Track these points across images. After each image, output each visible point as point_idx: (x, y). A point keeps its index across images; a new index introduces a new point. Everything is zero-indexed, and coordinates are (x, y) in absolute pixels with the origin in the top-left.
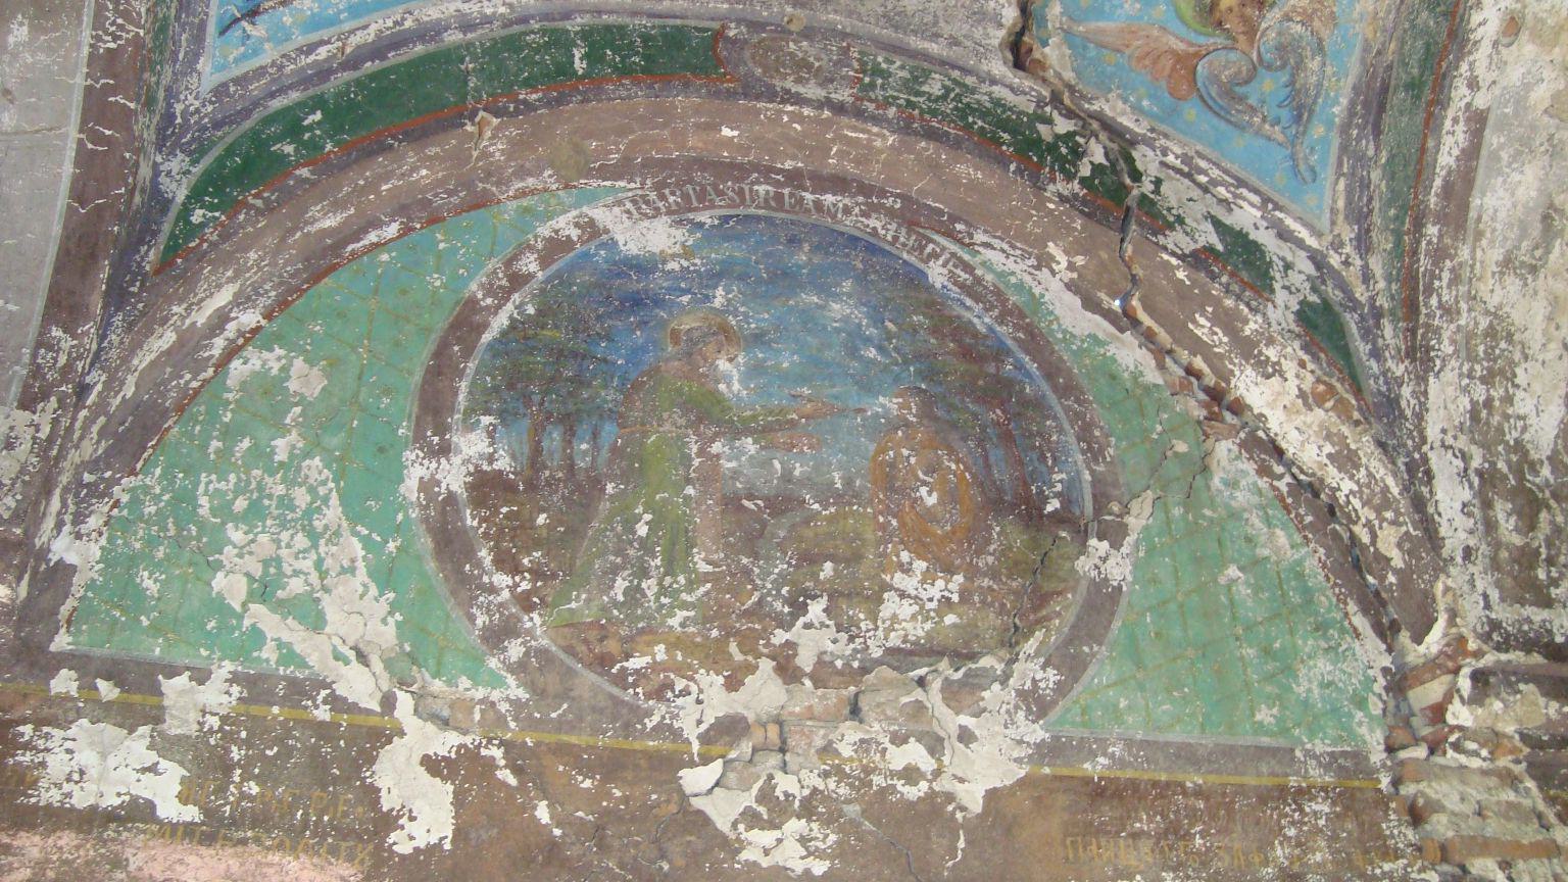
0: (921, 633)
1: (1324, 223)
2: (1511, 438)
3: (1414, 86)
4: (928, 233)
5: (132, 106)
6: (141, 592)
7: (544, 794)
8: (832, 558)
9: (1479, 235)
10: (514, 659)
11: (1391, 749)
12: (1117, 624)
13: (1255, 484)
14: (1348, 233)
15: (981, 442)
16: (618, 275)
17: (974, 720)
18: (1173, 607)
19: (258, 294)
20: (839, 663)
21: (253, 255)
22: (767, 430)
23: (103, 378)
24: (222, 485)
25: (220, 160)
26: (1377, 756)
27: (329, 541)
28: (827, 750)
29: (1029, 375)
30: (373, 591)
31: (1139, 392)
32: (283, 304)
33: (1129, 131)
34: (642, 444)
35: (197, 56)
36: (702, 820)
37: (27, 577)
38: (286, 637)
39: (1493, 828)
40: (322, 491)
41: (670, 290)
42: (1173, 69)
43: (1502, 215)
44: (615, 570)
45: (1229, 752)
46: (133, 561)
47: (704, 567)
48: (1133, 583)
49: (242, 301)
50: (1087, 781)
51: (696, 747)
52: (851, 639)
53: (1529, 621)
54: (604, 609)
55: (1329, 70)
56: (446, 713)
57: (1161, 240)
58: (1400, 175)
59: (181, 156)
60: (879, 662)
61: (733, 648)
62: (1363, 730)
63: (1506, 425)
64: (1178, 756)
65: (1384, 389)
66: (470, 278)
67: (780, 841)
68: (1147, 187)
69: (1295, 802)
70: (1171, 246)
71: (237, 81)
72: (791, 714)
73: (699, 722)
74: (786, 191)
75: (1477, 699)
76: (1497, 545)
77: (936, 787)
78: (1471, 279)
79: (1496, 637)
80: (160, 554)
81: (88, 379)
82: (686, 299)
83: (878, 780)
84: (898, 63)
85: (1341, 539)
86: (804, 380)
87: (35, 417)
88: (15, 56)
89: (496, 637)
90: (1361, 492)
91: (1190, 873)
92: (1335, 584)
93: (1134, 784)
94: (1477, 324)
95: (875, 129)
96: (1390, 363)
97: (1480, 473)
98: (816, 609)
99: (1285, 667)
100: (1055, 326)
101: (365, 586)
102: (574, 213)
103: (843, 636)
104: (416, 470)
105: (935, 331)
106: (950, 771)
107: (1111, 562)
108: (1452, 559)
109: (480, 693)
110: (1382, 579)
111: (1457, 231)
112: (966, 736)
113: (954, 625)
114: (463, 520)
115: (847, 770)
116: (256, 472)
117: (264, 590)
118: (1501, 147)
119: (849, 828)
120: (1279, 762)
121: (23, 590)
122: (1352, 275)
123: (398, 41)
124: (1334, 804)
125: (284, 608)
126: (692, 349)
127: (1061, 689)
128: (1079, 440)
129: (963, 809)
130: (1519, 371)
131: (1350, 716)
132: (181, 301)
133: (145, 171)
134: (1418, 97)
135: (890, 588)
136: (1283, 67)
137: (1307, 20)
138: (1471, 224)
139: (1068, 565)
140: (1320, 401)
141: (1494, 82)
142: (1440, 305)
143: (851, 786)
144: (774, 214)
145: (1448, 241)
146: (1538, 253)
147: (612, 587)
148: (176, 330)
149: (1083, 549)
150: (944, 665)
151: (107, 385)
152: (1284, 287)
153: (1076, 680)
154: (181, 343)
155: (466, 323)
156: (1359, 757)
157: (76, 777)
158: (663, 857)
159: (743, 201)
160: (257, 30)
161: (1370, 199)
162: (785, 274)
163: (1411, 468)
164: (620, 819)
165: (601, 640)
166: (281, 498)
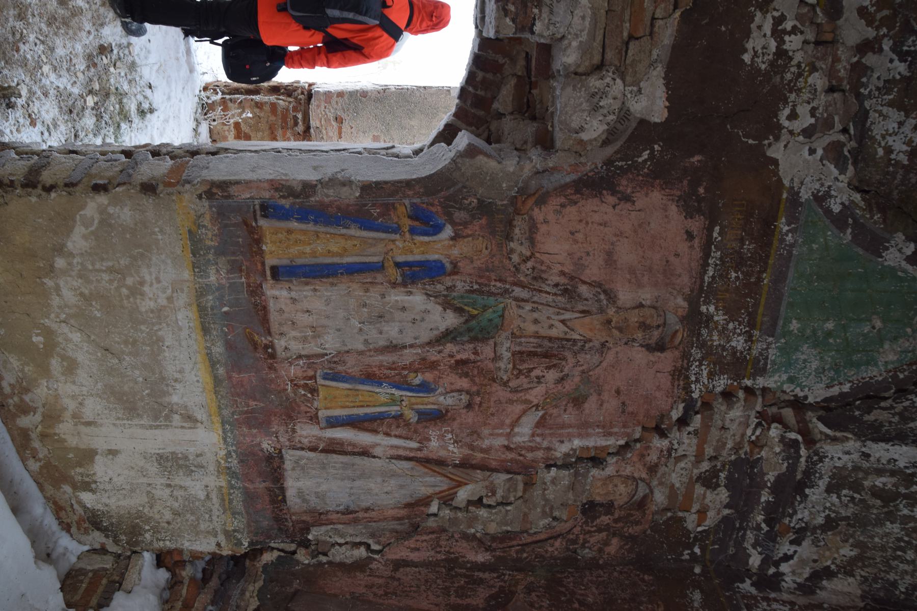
0: (875, 132)
11: (765, 390)
12: (860, 251)
17: (819, 158)
20: (864, 80)
26: (761, 382)
28: (813, 69)
39: (715, 433)
48: (882, 265)
50: (775, 219)
52: (878, 89)
53: (821, 478)
60: (861, 105)
61: (886, 12)
62: (776, 378)
67: (765, 35)
72: (838, 49)
75: (782, 439)
76: (867, 472)
79: (815, 458)
83: (793, 96)
85: (885, 392)
91: (718, 267)
92: (860, 382)
93: (769, 244)
103: (881, 84)
107: (898, 255)
108: (865, 446)
110: (858, 408)
112: (812, 152)
113: (876, 153)
115: (801, 80)
124: (742, 353)
127: (828, 212)
129: (770, 145)
131: (786, 372)
135: (907, 116)
143: (790, 81)
150: (853, 144)
153: (832, 221)
156: (762, 371)
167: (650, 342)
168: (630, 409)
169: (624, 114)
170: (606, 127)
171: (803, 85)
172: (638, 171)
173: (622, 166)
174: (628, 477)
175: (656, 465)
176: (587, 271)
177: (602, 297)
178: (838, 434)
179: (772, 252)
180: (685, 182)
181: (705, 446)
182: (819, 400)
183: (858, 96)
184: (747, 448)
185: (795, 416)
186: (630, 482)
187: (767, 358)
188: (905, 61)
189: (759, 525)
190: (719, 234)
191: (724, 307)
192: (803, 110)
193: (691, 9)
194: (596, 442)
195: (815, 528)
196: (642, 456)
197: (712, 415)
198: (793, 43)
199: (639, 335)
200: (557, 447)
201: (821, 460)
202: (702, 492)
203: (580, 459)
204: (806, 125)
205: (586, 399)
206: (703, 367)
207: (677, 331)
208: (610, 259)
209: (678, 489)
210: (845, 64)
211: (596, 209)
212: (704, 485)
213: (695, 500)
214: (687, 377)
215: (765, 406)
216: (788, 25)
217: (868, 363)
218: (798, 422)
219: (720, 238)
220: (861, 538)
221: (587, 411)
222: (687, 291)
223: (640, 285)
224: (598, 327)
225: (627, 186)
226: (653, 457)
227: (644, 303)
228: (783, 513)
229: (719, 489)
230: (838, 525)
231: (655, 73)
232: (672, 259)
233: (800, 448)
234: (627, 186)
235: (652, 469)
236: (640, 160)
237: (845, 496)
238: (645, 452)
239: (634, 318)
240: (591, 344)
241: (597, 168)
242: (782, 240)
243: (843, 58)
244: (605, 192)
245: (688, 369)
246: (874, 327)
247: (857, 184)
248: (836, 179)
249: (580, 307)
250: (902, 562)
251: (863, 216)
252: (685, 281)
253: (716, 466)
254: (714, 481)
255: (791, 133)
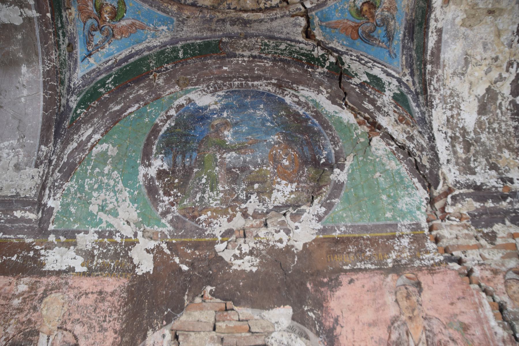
1: (400, 70)
2: (461, 126)
3: (420, 24)
4: (285, 88)
5: (55, 84)
6: (70, 212)
7: (177, 255)
8: (258, 183)
9: (444, 66)
10: (169, 219)
11: (428, 221)
13: (385, 148)
14: (407, 71)
15: (301, 146)
16: (197, 112)
18: (360, 186)
19: (99, 130)
20: (260, 212)
21: (96, 120)
22: (239, 149)
23: (56, 157)
24: (91, 182)
25: (85, 96)
26: (424, 224)
27: (119, 193)
28: (257, 236)
29: (316, 125)
30: (131, 204)
31: (349, 126)
32: (106, 132)
33: (340, 51)
34: (204, 157)
35: (76, 68)
36: (221, 259)
37: (41, 212)
38: (108, 220)
39: (461, 242)
40: (117, 180)
41: (211, 114)
42: (352, 31)
43: (451, 58)
44: (197, 192)
45: (377, 226)
46: (68, 205)
47: (221, 189)
49: (94, 132)
50: (334, 238)
51: (220, 238)
52: (263, 205)
53: (469, 180)
54: (194, 204)
55: (397, 24)
56: (152, 236)
57: (350, 81)
58: (419, 51)
59: (74, 96)
60: (272, 210)
61: (230, 210)
62: (420, 217)
63: (459, 122)
64: (362, 229)
65: (420, 116)
66: (156, 118)
67: (243, 263)
68: (346, 67)
69: (398, 239)
70: (353, 82)
71: (87, 74)
73: (220, 232)
74: (244, 82)
75: (453, 205)
76: (458, 158)
77: (289, 244)
78: (443, 80)
79: (458, 185)
80: (75, 202)
81: (52, 158)
82: (215, 116)
83: (271, 243)
84: (272, 42)
86: (249, 134)
87: (39, 170)
88: (24, 75)
89: (164, 214)
90: (416, 147)
91: (366, 262)
93: (348, 239)
94: (446, 93)
95: (266, 61)
96: (422, 108)
97: (451, 137)
98: (253, 197)
99: (394, 200)
100: (323, 110)
101: (129, 204)
102: (184, 97)
103: (261, 204)
104: (142, 170)
105: (288, 116)
106: (292, 239)
107: (341, 175)
109: (160, 229)
110: (424, 171)
111: (437, 66)
112: (297, 228)
114: (155, 183)
116: (100, 177)
117: (102, 208)
118: (448, 38)
119: (263, 257)
120: (393, 228)
121: (40, 215)
122: (410, 84)
123: (131, 56)
124: (410, 239)
125: (109, 213)
126: (218, 130)
127: (326, 213)
128: (331, 141)
129: (296, 249)
130: (461, 105)
131: (415, 213)
132: (77, 134)
133: (63, 101)
134: (421, 27)
135: (275, 189)
136: (384, 25)
137: (389, 10)
138: (441, 63)
139: (328, 177)
140: (401, 121)
141: (443, 19)
142: (434, 89)
143: (264, 246)
144: (240, 89)
145: (434, 69)
146: (464, 69)
147: (195, 197)
148: (77, 142)
149: (332, 172)
150: (291, 209)
151: (58, 159)
152: (389, 90)
153: (330, 210)
154: (79, 145)
155: (155, 130)
156: (418, 226)
157: (55, 262)
158: (210, 270)
159: (231, 87)
160: (91, 60)
161: (413, 60)
162: (244, 105)
163: (429, 138)
164: (199, 260)
165: (193, 212)
166: (106, 183)
167: (417, 291)
168: (461, 294)
169: (291, 329)
170: (298, 339)
171: (265, 239)
172: (320, 316)
173: (319, 326)
174: (506, 286)
175: (492, 270)
176: (383, 336)
177: (396, 325)
178: (441, 177)
179: (351, 236)
180: (322, 289)
181: (471, 245)
182: (426, 192)
183: (267, 213)
184: (464, 222)
185: (438, 201)
186: (509, 284)
187: (410, 225)
188: (250, 196)
189: (509, 203)
190: (347, 265)
191: (387, 254)
192: (277, 237)
193: (233, 302)
194: (488, 311)
195: (499, 174)
196: (489, 280)
197: (451, 246)
198: (246, 248)
199: (414, 298)
200: (500, 336)
201: (458, 182)
202: (500, 239)
203: (504, 319)
204: (284, 234)
205: (462, 323)
206: (424, 258)
207: (407, 277)
208: (373, 324)
209: (503, 254)
210: (253, 222)
211: (345, 338)
212: (495, 240)
213: (507, 242)
214: (432, 265)
215: (437, 218)
216: (237, 252)
217: (399, 174)
218: (441, 199)
219: (350, 265)
220: (496, 150)
221: (470, 321)
222: (382, 277)
223: (385, 304)
224: (415, 324)
225: (329, 322)
226: (488, 274)
227: (394, 300)
228: (496, 192)
229: (495, 230)
230: (493, 163)
231: (267, 316)
232: (366, 288)
233: (456, 195)
234: (329, 322)
235: (495, 272)
236: (314, 317)
237: (474, 164)
238: (486, 279)
239: (404, 303)
240: (427, 326)
241: (322, 341)
242: (345, 232)
243: (251, 224)
244: (335, 334)
245: (427, 266)
246: (380, 176)
247: (310, 203)
248: (309, 213)
249: (405, 337)
250: (501, 128)
251: (325, 196)
252: (377, 279)
253: (481, 236)
254: (490, 234)
255: (289, 240)
